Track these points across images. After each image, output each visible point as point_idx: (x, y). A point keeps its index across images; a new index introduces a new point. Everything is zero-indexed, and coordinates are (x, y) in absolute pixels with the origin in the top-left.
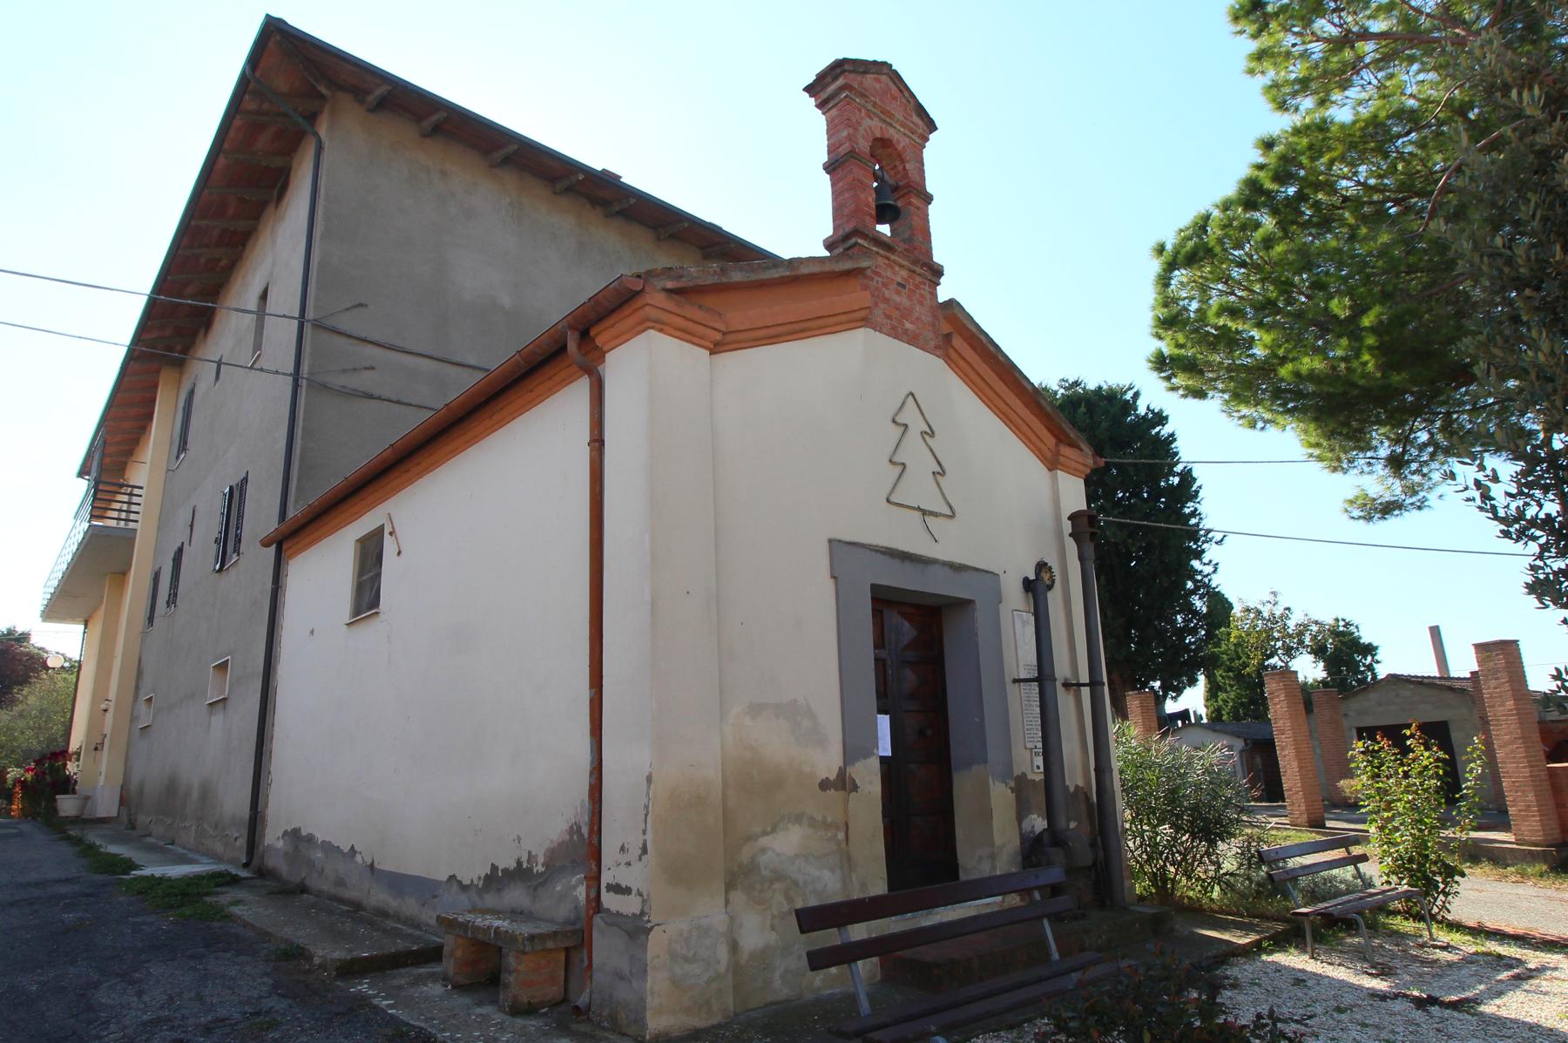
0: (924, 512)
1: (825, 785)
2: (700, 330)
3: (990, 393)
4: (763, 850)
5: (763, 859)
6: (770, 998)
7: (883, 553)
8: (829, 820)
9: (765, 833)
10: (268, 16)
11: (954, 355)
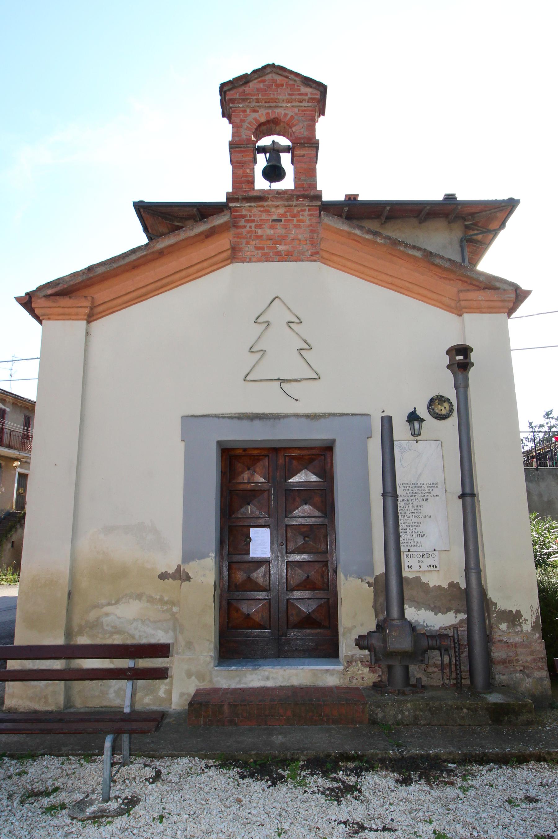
0: (283, 381)
1: (163, 576)
2: (73, 310)
3: (183, 273)
4: (107, 614)
5: (105, 620)
6: (105, 703)
7: (219, 418)
8: (166, 599)
9: (109, 604)
10: (134, 203)
11: (326, 255)
